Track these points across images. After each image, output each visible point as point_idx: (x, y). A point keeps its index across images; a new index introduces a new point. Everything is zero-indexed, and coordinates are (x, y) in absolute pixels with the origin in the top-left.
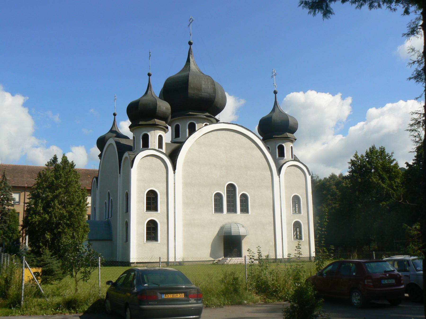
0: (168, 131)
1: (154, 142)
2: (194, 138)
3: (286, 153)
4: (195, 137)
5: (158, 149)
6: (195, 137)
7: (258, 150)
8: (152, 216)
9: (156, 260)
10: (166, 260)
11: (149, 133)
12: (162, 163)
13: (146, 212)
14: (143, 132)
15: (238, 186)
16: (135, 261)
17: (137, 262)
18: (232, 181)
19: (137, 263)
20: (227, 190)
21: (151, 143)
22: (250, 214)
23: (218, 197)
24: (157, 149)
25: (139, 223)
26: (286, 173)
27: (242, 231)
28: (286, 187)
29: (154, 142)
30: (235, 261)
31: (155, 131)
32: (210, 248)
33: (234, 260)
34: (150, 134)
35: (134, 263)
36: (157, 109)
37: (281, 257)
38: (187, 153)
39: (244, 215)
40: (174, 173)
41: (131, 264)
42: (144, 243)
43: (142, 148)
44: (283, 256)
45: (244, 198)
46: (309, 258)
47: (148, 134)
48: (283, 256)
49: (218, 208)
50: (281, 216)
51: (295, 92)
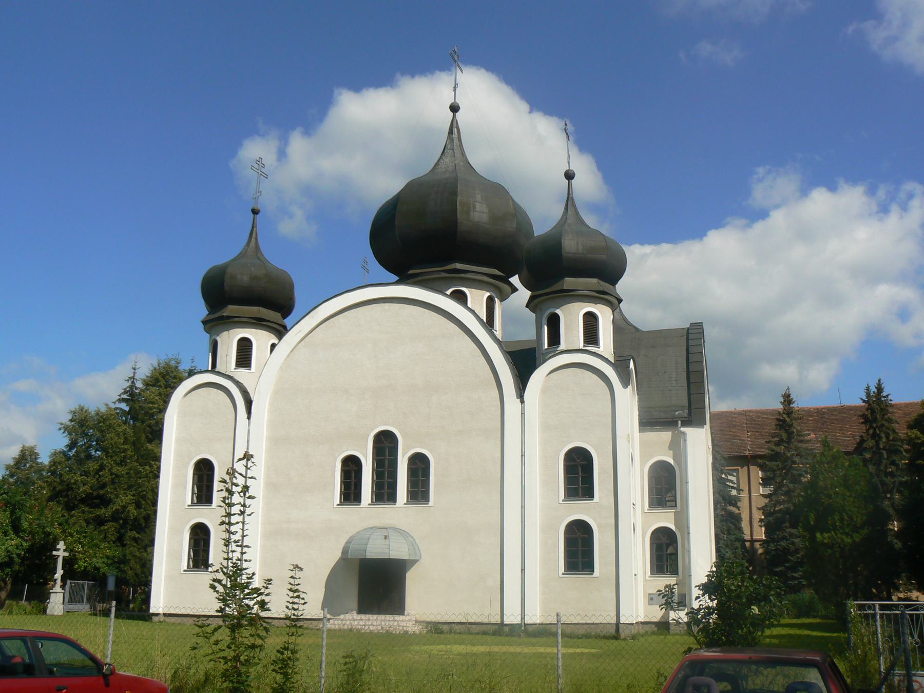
0: (620, 301)
1: (227, 355)
2: (297, 334)
3: (566, 334)
4: (300, 331)
5: (584, 346)
6: (300, 331)
7: (466, 337)
8: (580, 511)
9: (475, 619)
10: (499, 622)
11: (558, 310)
12: (228, 398)
13: (563, 501)
14: (547, 310)
15: (402, 435)
16: (161, 611)
17: (164, 612)
18: (388, 425)
19: (165, 615)
20: (374, 447)
21: (221, 357)
22: (431, 502)
23: (351, 466)
24: (581, 346)
25: (175, 531)
26: (545, 390)
27: (397, 550)
28: (546, 427)
29: (227, 355)
30: (375, 623)
31: (231, 331)
32: (324, 590)
33: (375, 622)
34: (220, 339)
35: (157, 615)
36: (225, 285)
37: (517, 620)
38: (281, 368)
39: (417, 509)
40: (249, 418)
41: (153, 617)
42: (646, 580)
43: (546, 346)
44: (523, 618)
45: (419, 465)
46: (615, 625)
47: (556, 312)
48: (523, 618)
49: (350, 493)
50: (523, 507)
51: (597, 162)
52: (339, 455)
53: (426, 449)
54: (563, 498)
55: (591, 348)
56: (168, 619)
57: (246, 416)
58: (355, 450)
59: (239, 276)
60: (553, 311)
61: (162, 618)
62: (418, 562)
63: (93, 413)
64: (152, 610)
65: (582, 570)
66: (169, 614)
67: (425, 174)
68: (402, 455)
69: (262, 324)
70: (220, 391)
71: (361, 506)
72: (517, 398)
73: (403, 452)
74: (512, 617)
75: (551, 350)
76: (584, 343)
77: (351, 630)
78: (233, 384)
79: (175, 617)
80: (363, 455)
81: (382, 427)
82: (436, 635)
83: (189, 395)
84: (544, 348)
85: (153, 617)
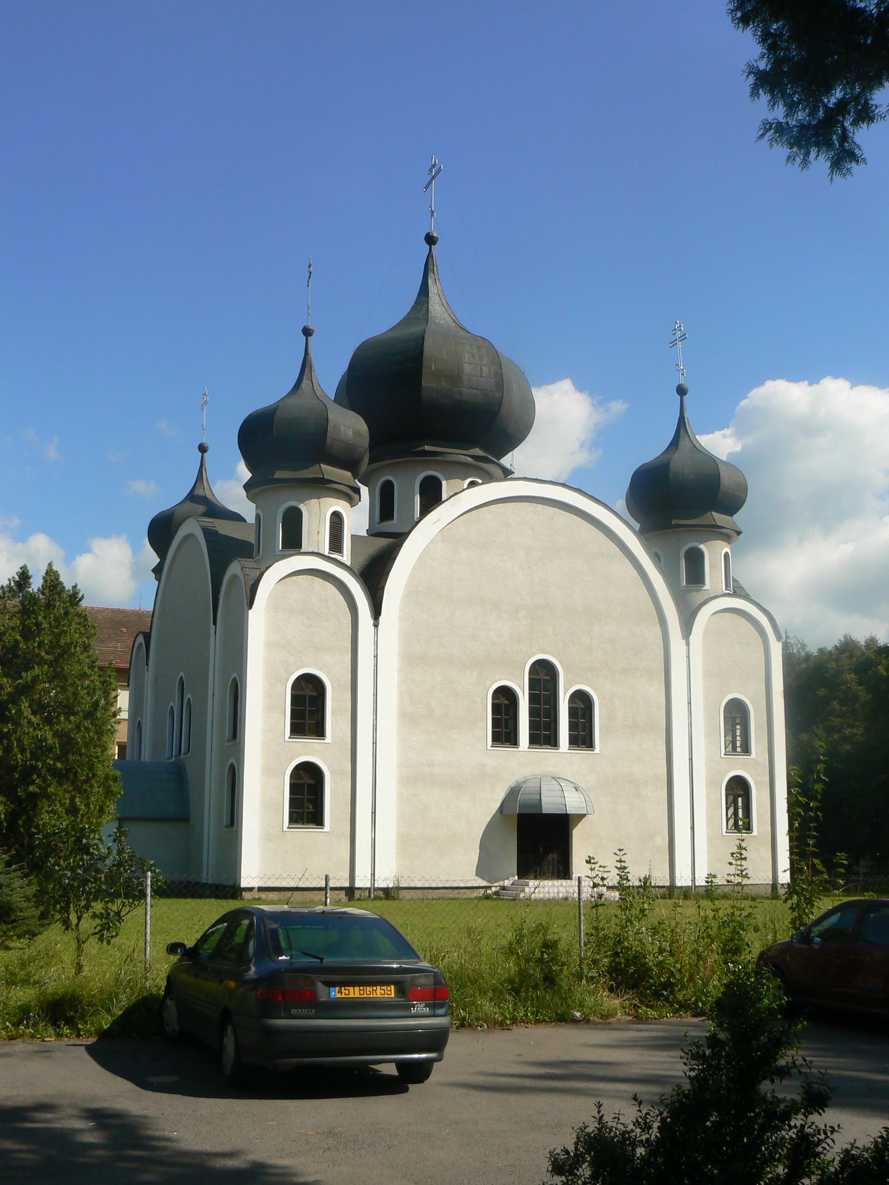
1: (318, 533)
5: (329, 553)
11: (702, 545)
16: (255, 884)
19: (261, 889)
22: (597, 750)
25: (269, 772)
27: (573, 803)
28: (708, 674)
29: (318, 533)
31: (323, 500)
35: (251, 889)
39: (581, 754)
40: (376, 626)
41: (244, 893)
43: (280, 549)
44: (693, 880)
48: (693, 880)
52: (491, 685)
53: (589, 686)
54: (289, 735)
55: (335, 556)
56: (263, 895)
57: (372, 622)
58: (510, 680)
59: (342, 427)
60: (296, 505)
61: (256, 895)
62: (585, 818)
63: (863, 643)
64: (244, 884)
65: (307, 823)
66: (340, 887)
67: (393, 326)
68: (564, 691)
69: (713, 531)
70: (328, 583)
71: (520, 749)
72: (683, 639)
73: (564, 688)
74: (683, 879)
75: (284, 553)
76: (330, 550)
77: (566, 899)
78: (752, 605)
79: (273, 891)
80: (520, 687)
81: (540, 655)
82: (663, 900)
83: (727, 615)
84: (277, 550)
85: (244, 893)
